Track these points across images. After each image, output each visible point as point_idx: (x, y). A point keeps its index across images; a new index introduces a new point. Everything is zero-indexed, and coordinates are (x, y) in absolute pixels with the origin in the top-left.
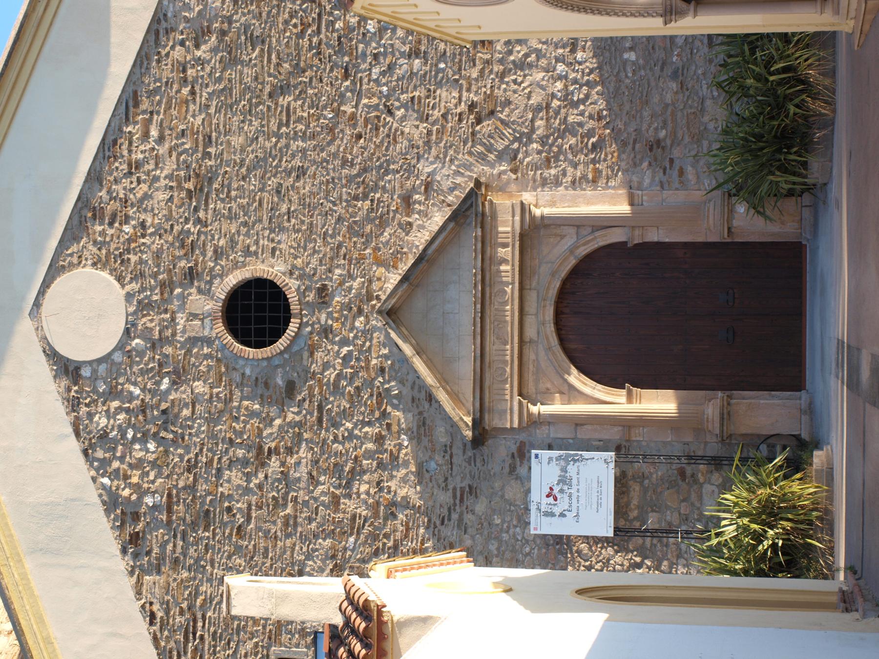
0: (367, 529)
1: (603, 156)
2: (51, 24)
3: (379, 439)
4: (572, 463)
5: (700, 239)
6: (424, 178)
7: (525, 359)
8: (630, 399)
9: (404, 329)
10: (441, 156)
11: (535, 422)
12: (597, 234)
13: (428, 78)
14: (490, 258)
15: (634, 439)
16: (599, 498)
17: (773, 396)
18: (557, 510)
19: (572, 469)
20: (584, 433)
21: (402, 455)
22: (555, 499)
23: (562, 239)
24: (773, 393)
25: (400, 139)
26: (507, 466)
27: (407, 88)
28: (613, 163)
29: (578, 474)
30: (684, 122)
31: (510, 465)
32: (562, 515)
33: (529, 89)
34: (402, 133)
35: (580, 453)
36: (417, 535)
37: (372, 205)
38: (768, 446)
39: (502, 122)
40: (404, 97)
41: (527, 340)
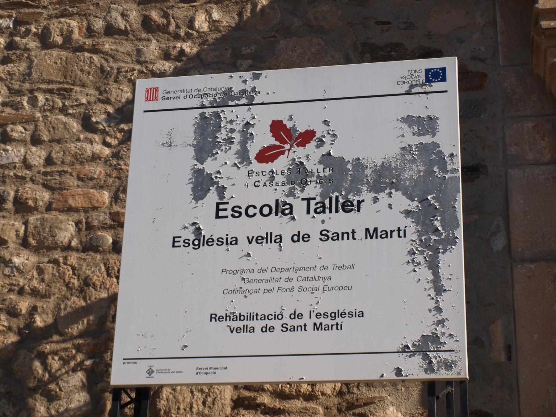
4: (414, 205)
29: (370, 233)
35: (460, 233)
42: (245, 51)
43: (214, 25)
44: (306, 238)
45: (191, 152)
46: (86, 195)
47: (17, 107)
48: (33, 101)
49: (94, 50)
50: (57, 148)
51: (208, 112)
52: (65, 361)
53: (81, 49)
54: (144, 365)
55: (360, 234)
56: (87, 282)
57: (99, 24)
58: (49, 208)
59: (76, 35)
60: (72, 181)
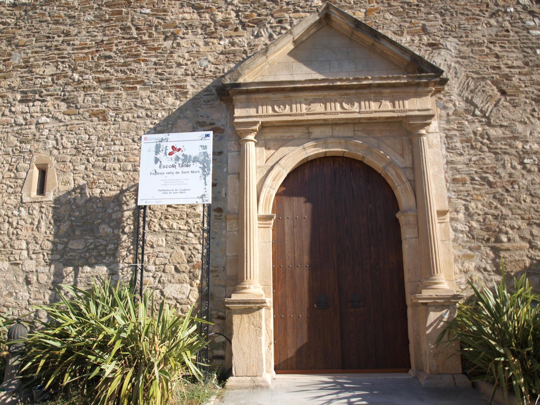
0: (155, 21)
1: (477, 186)
2: (245, 303)
3: (225, 24)
4: (202, 166)
5: (407, 277)
6: (441, 42)
7: (294, 129)
8: (264, 218)
9: (314, 30)
10: (462, 55)
11: (240, 138)
12: (408, 185)
13: (525, 41)
14: (380, 93)
15: (228, 223)
16: (170, 191)
17: (269, 347)
18: (161, 156)
19: (196, 167)
20: (231, 180)
21: (212, 40)
22: (170, 154)
23: (400, 155)
24: (272, 346)
25: (471, 23)
26: (204, 119)
27: (515, 27)
28: (472, 196)
29: (192, 172)
30: (517, 258)
31: (204, 122)
32: (157, 160)
33: (528, 122)
34: (477, 25)
35: (211, 172)
36: (150, 56)
37: (414, 5)
38: (223, 342)
39: (498, 101)
40: (507, 24)
41: (310, 130)
42: (170, 123)
43: (163, 116)
44: (179, 173)
45: (154, 153)
46: (134, 158)
47: (117, 136)
48: (121, 135)
49: (135, 122)
50: (127, 146)
51: (158, 143)
52: (130, 197)
53: (131, 121)
54: (145, 201)
55: (190, 172)
56: (134, 179)
57: (136, 115)
58: (125, 161)
59: (130, 118)
60: (130, 155)
